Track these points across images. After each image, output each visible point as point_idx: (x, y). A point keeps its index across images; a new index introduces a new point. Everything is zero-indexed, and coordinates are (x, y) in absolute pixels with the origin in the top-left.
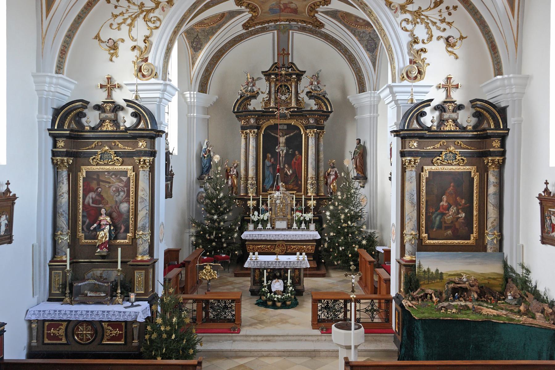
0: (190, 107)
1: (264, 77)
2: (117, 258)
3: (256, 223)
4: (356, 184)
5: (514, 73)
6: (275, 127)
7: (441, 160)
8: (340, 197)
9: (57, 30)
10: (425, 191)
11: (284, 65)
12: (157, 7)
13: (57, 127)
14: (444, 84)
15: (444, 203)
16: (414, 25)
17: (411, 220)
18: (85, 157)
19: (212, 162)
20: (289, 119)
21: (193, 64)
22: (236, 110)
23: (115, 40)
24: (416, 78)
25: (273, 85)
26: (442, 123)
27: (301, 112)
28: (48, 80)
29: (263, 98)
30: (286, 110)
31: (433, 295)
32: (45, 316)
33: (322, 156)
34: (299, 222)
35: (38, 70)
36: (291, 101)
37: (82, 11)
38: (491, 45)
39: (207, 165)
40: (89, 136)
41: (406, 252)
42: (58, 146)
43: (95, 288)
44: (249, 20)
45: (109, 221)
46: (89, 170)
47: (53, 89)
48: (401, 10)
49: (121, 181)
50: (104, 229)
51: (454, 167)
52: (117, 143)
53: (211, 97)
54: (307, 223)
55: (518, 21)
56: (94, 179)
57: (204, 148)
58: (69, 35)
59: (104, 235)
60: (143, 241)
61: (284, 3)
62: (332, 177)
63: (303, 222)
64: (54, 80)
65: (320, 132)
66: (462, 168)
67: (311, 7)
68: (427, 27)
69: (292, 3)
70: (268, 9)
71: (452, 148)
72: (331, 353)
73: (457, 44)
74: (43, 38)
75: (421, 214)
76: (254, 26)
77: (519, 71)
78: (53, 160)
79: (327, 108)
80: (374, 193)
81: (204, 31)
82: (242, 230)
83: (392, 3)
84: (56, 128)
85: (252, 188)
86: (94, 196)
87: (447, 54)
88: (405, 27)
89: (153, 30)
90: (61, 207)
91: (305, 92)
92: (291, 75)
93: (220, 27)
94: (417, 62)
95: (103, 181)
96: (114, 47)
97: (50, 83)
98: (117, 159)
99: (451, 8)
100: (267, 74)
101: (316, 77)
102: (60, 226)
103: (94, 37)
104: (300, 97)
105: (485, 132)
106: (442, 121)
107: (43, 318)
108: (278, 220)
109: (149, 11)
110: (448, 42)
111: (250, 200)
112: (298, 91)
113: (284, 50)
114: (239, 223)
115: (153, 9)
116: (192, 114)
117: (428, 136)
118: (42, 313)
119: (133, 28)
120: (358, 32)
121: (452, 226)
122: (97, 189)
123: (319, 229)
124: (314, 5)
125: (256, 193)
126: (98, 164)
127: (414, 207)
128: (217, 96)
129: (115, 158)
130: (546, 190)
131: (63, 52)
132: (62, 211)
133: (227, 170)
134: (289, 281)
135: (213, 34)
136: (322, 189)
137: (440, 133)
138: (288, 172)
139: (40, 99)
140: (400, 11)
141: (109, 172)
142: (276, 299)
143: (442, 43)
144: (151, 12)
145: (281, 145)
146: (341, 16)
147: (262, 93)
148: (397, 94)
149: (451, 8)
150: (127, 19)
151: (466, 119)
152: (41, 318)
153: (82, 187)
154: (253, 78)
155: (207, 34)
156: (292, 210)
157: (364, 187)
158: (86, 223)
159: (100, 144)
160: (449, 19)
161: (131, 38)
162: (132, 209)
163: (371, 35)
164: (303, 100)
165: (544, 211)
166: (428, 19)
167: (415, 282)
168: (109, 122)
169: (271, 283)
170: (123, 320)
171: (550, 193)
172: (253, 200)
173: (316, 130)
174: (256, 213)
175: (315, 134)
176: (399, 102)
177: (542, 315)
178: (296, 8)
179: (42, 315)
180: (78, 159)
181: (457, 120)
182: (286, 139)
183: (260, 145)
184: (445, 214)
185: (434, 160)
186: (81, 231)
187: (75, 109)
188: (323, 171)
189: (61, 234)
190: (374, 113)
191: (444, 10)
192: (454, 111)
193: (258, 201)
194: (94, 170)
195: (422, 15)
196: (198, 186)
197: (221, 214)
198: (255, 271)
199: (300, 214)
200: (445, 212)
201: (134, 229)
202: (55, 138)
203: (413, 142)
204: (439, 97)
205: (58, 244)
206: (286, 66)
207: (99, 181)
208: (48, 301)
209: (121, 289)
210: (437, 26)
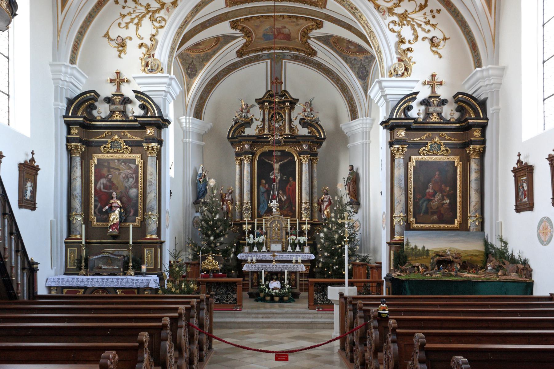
0: (185, 133)
1: (256, 104)
2: (129, 239)
3: (251, 246)
4: (349, 208)
5: (492, 64)
6: (269, 154)
7: (427, 151)
8: (333, 219)
9: (71, 26)
10: (412, 179)
11: (277, 93)
12: (162, 7)
13: (72, 114)
14: (429, 80)
15: (430, 190)
16: (401, 27)
17: (400, 204)
18: (96, 146)
19: (207, 187)
20: (283, 146)
21: (188, 90)
22: (230, 137)
23: (124, 37)
24: (403, 74)
25: (266, 112)
26: (428, 116)
27: (294, 138)
28: (63, 69)
29: (257, 126)
30: (280, 136)
31: (420, 267)
32: (64, 283)
33: (315, 183)
34: (294, 245)
35: (54, 60)
36: (285, 129)
37: (93, 9)
38: (471, 45)
39: (203, 189)
40: (100, 126)
41: (395, 233)
42: (72, 133)
43: (108, 260)
44: (243, 47)
45: (120, 204)
46: (100, 158)
47: (67, 79)
48: (389, 13)
49: (130, 168)
50: (115, 211)
51: (439, 157)
53: (206, 123)
54: (302, 246)
55: (495, 19)
57: (199, 173)
58: (81, 32)
59: (115, 217)
60: (152, 221)
61: (278, 28)
62: (326, 204)
63: (298, 245)
64: (69, 71)
65: (313, 159)
66: (446, 158)
67: (304, 32)
68: (414, 30)
69: (285, 27)
70: (262, 34)
71: (437, 140)
72: (327, 324)
73: (440, 44)
74: (59, 32)
75: (409, 200)
76: (248, 54)
77: (497, 63)
78: (67, 146)
79: (320, 135)
80: (366, 219)
81: (199, 57)
82: (239, 250)
83: (381, 5)
84: (70, 115)
85: (247, 213)
86: (105, 182)
87: (432, 54)
88: (392, 28)
89: (158, 29)
90: (75, 190)
91: (298, 120)
92: (284, 102)
93: (214, 53)
94: (404, 59)
96: (122, 45)
97: (66, 73)
98: (127, 148)
99: (435, 11)
100: (260, 102)
101: (309, 104)
102: (74, 207)
103: (103, 35)
104: (293, 125)
105: (467, 122)
106: (428, 114)
107: (62, 284)
108: (273, 243)
109: (154, 12)
110: (433, 42)
111: (245, 224)
112: (291, 119)
113: (277, 78)
114: (235, 245)
115: (158, 10)
116: (187, 140)
117: (414, 127)
118: (61, 280)
119: (139, 27)
120: (350, 59)
121: (437, 211)
122: (108, 175)
123: (314, 250)
124: (307, 29)
125: (251, 218)
126: (108, 153)
127: (402, 191)
128: (212, 124)
129: (124, 147)
130: (519, 162)
131: (76, 48)
132: (76, 193)
133: (222, 196)
134: (286, 282)
135: (208, 60)
136: (316, 215)
137: (425, 125)
138: (282, 197)
139: (56, 87)
140: (388, 13)
141: (119, 160)
142: (274, 294)
143: (427, 43)
144: (156, 12)
145: (276, 171)
146: (333, 42)
147: (256, 120)
148: (385, 89)
149: (435, 11)
150: (134, 18)
151: (449, 112)
152: (60, 285)
153: (94, 173)
154: (247, 105)
155: (201, 60)
156: (287, 234)
157: (356, 213)
158: (98, 207)
159: (110, 134)
160: (433, 21)
161: (139, 36)
162: (141, 194)
163: (363, 62)
164: (296, 128)
165: (517, 182)
166: (414, 21)
167: (403, 258)
168: (119, 114)
169: (269, 284)
170: (136, 287)
171: (522, 162)
172: (249, 224)
173: (309, 155)
174: (251, 236)
175: (309, 160)
176: (388, 97)
177: (517, 274)
178: (289, 33)
179: (61, 282)
180: (90, 148)
181: (441, 113)
182: (281, 166)
183: (255, 171)
184: (431, 200)
185: (421, 151)
186: (93, 214)
187: (87, 100)
188: (317, 197)
189: (75, 215)
190: (366, 139)
191: (428, 13)
192: (438, 106)
193: (253, 224)
194: (105, 158)
195: (409, 17)
196: (194, 211)
197: (217, 236)
198: (253, 275)
199: (294, 237)
200: (431, 198)
201: (142, 213)
202: (69, 125)
203: (401, 131)
204: (425, 93)
205: (73, 223)
206: (280, 94)
207: (109, 168)
209: (132, 263)
210: (422, 28)
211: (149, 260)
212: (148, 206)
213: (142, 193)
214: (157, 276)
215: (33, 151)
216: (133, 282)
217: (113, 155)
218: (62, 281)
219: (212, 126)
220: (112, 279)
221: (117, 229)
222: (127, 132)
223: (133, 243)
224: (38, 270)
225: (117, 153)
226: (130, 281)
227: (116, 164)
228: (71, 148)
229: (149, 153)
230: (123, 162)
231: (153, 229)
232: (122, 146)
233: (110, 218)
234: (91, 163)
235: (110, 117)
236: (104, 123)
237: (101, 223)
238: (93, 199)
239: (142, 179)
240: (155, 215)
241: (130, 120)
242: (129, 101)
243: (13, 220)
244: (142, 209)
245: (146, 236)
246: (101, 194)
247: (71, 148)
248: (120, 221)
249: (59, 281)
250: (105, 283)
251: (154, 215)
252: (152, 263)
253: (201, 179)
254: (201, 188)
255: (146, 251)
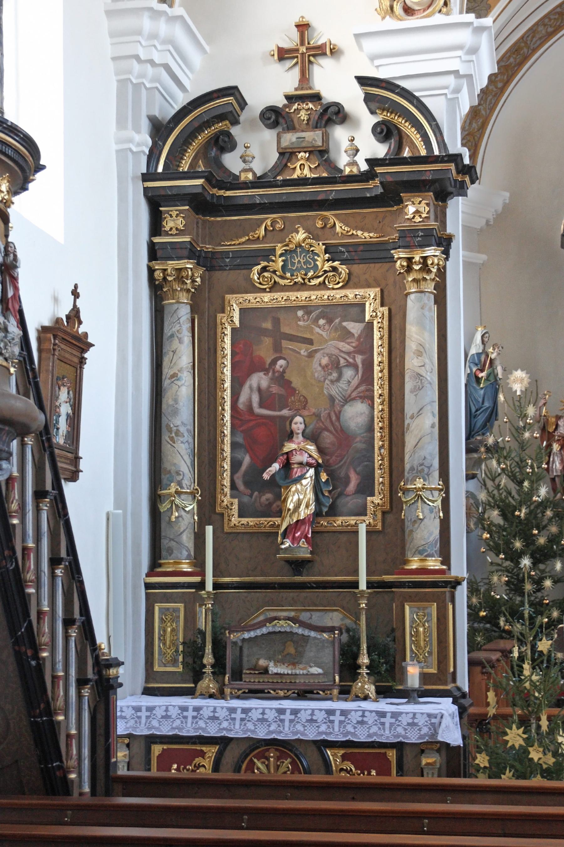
18: (238, 267)
28: (147, 23)
32: (155, 723)
39: (487, 404)
42: (167, 229)
45: (315, 455)
49: (346, 335)
50: (302, 477)
52: (331, 221)
56: (265, 332)
64: (163, 28)
78: (151, 271)
84: (160, 169)
90: (175, 412)
95: (292, 338)
97: (153, 36)
98: (334, 269)
102: (173, 469)
107: (149, 729)
118: (144, 714)
122: (274, 362)
126: (275, 287)
128: (507, 194)
132: (179, 423)
139: (122, 84)
141: (307, 309)
152: (142, 731)
153: (229, 357)
158: (244, 467)
168: (308, 159)
179: (143, 720)
180: (218, 275)
186: (227, 490)
189: (178, 493)
205: (170, 521)
208: (143, 693)
211: (422, 644)
212: (409, 461)
213: (386, 415)
214: (453, 703)
215: (76, 286)
216: (383, 724)
217: (293, 295)
218: (148, 717)
219: (507, 201)
220: (309, 712)
221: (306, 537)
222: (335, 215)
223: (370, 585)
224: (121, 685)
225: (303, 286)
226: (370, 719)
227: (301, 323)
228: (165, 279)
229: (414, 280)
230: (322, 315)
231: (431, 539)
232: (319, 264)
233: (285, 500)
234: (222, 324)
235: (278, 170)
236: (261, 191)
237: (251, 521)
238: (228, 440)
239: (386, 371)
240: (435, 489)
241: (348, 176)
242: (341, 115)
243: (62, 513)
244: (387, 470)
245: (406, 562)
246: (251, 424)
247: (165, 279)
248: (318, 514)
249: (139, 717)
250: (287, 723)
251: (431, 490)
252: (430, 653)
253: (482, 371)
254: (480, 400)
255: (411, 613)
